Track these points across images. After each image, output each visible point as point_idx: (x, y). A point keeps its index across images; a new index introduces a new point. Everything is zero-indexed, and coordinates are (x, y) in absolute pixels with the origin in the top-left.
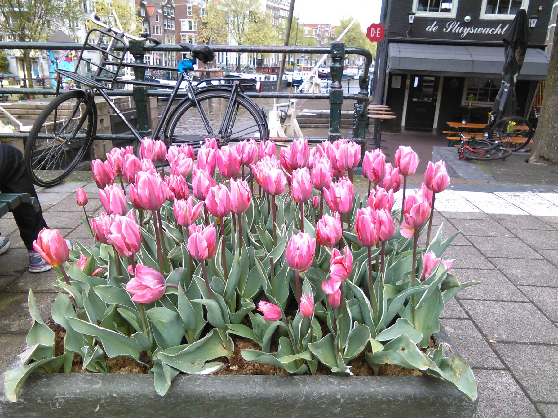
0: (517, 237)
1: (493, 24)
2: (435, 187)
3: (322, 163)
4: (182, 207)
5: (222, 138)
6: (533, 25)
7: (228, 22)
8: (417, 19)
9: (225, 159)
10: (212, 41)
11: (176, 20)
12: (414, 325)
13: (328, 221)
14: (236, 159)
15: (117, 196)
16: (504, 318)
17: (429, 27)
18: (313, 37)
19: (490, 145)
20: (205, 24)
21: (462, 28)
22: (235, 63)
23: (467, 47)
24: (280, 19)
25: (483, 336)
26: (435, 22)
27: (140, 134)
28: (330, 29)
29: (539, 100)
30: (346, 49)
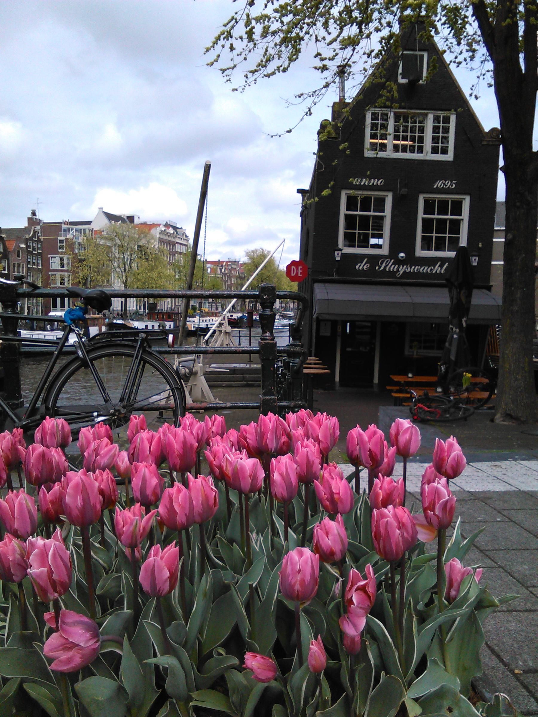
0: (512, 521)
1: (432, 261)
2: (449, 471)
3: (307, 446)
4: (129, 521)
5: (124, 407)
6: (475, 264)
7: (111, 259)
8: (344, 256)
9: (177, 446)
10: (91, 282)
11: (43, 256)
12: (445, 665)
13: (329, 528)
14: (192, 445)
15: (25, 506)
16: (523, 636)
17: (359, 265)
18: (219, 276)
19: (447, 403)
20: (81, 261)
21: (397, 266)
22: (119, 308)
23: (407, 288)
24: (176, 255)
25: (505, 664)
26: (366, 260)
27: (8, 405)
28: (237, 267)
29: (491, 345)
30: (277, 293)
